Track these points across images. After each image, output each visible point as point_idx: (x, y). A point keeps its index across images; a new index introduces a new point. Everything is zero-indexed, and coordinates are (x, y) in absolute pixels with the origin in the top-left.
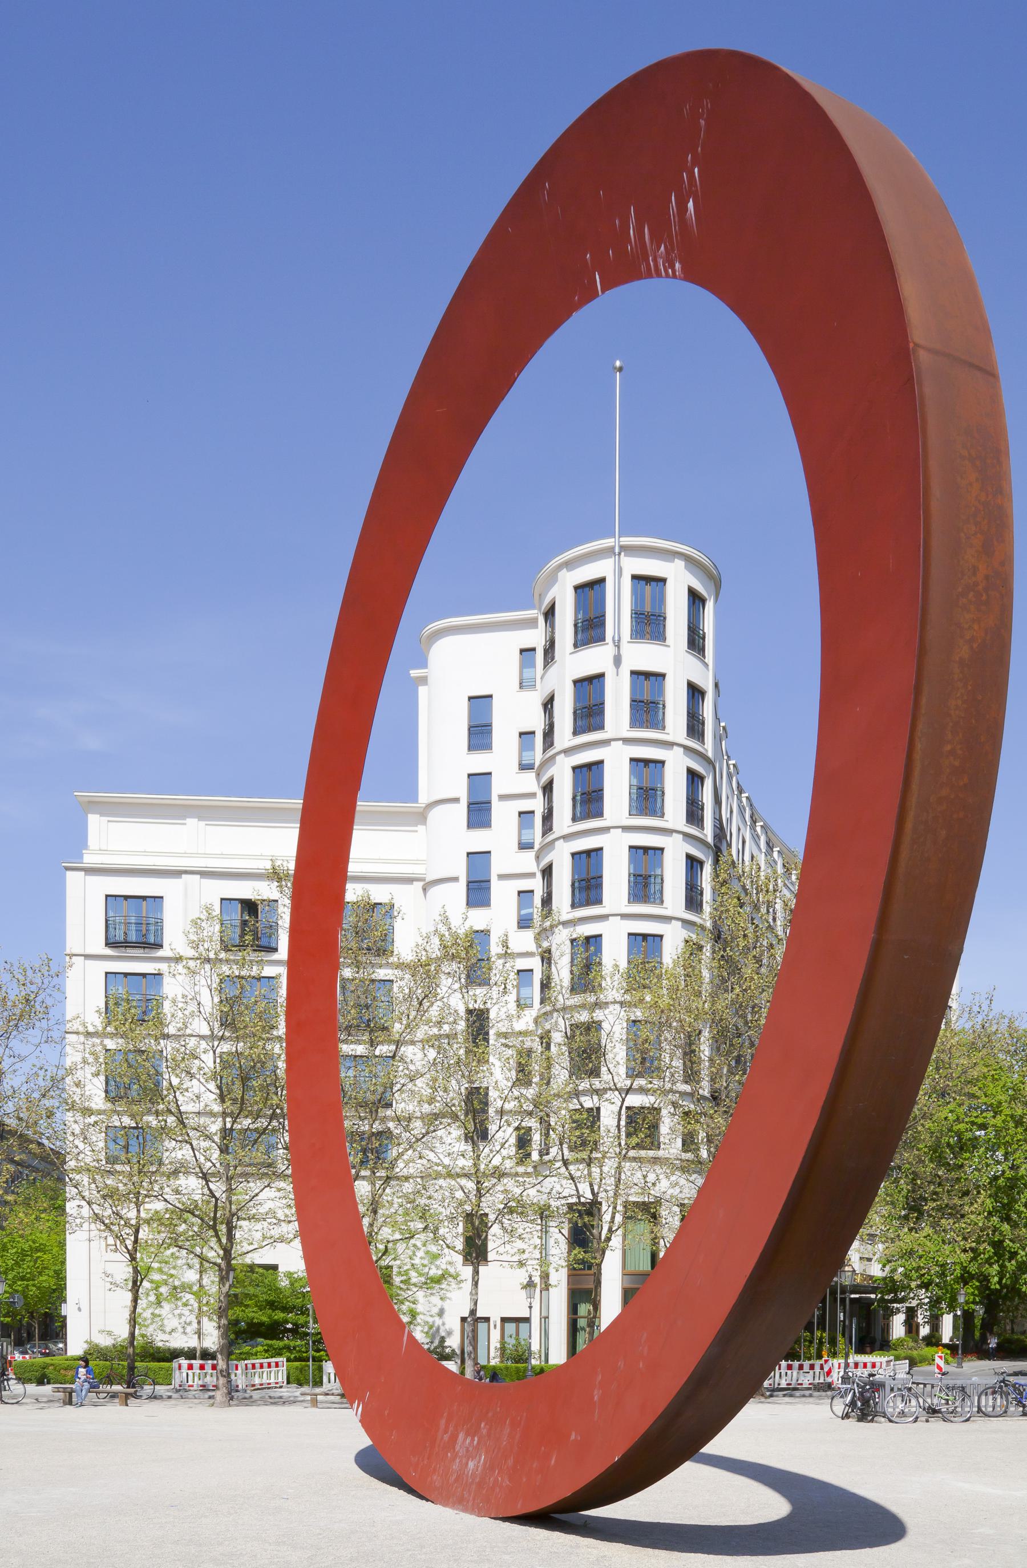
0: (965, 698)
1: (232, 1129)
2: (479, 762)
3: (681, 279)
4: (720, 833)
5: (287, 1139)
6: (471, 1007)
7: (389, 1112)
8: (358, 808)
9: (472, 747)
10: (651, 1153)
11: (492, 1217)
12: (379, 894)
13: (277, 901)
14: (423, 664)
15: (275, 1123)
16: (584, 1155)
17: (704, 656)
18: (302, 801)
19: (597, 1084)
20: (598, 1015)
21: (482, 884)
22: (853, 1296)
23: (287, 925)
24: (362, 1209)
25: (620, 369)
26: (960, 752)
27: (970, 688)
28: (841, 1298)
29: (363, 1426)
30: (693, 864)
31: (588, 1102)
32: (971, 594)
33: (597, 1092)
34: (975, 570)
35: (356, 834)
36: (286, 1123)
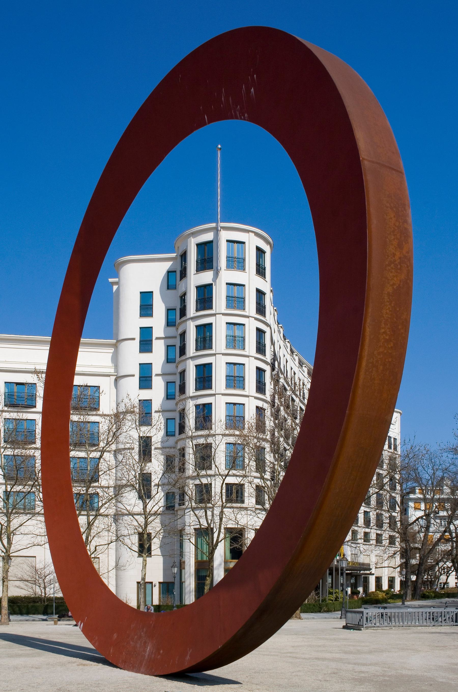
0: (391, 309)
1: (10, 492)
2: (146, 322)
3: (248, 121)
4: (275, 358)
5: (41, 497)
6: (141, 435)
7: (96, 484)
8: (81, 341)
9: (142, 315)
10: (239, 505)
11: (153, 535)
13: (36, 384)
14: (117, 275)
15: (34, 489)
16: (203, 505)
17: (265, 278)
18: (51, 338)
19: (209, 472)
21: (147, 378)
22: (347, 572)
23: (42, 395)
24: (82, 530)
25: (220, 149)
26: (389, 333)
27: (393, 305)
28: (341, 573)
30: (260, 371)
31: (204, 481)
32: (392, 265)
33: (210, 476)
34: (394, 255)
36: (41, 489)
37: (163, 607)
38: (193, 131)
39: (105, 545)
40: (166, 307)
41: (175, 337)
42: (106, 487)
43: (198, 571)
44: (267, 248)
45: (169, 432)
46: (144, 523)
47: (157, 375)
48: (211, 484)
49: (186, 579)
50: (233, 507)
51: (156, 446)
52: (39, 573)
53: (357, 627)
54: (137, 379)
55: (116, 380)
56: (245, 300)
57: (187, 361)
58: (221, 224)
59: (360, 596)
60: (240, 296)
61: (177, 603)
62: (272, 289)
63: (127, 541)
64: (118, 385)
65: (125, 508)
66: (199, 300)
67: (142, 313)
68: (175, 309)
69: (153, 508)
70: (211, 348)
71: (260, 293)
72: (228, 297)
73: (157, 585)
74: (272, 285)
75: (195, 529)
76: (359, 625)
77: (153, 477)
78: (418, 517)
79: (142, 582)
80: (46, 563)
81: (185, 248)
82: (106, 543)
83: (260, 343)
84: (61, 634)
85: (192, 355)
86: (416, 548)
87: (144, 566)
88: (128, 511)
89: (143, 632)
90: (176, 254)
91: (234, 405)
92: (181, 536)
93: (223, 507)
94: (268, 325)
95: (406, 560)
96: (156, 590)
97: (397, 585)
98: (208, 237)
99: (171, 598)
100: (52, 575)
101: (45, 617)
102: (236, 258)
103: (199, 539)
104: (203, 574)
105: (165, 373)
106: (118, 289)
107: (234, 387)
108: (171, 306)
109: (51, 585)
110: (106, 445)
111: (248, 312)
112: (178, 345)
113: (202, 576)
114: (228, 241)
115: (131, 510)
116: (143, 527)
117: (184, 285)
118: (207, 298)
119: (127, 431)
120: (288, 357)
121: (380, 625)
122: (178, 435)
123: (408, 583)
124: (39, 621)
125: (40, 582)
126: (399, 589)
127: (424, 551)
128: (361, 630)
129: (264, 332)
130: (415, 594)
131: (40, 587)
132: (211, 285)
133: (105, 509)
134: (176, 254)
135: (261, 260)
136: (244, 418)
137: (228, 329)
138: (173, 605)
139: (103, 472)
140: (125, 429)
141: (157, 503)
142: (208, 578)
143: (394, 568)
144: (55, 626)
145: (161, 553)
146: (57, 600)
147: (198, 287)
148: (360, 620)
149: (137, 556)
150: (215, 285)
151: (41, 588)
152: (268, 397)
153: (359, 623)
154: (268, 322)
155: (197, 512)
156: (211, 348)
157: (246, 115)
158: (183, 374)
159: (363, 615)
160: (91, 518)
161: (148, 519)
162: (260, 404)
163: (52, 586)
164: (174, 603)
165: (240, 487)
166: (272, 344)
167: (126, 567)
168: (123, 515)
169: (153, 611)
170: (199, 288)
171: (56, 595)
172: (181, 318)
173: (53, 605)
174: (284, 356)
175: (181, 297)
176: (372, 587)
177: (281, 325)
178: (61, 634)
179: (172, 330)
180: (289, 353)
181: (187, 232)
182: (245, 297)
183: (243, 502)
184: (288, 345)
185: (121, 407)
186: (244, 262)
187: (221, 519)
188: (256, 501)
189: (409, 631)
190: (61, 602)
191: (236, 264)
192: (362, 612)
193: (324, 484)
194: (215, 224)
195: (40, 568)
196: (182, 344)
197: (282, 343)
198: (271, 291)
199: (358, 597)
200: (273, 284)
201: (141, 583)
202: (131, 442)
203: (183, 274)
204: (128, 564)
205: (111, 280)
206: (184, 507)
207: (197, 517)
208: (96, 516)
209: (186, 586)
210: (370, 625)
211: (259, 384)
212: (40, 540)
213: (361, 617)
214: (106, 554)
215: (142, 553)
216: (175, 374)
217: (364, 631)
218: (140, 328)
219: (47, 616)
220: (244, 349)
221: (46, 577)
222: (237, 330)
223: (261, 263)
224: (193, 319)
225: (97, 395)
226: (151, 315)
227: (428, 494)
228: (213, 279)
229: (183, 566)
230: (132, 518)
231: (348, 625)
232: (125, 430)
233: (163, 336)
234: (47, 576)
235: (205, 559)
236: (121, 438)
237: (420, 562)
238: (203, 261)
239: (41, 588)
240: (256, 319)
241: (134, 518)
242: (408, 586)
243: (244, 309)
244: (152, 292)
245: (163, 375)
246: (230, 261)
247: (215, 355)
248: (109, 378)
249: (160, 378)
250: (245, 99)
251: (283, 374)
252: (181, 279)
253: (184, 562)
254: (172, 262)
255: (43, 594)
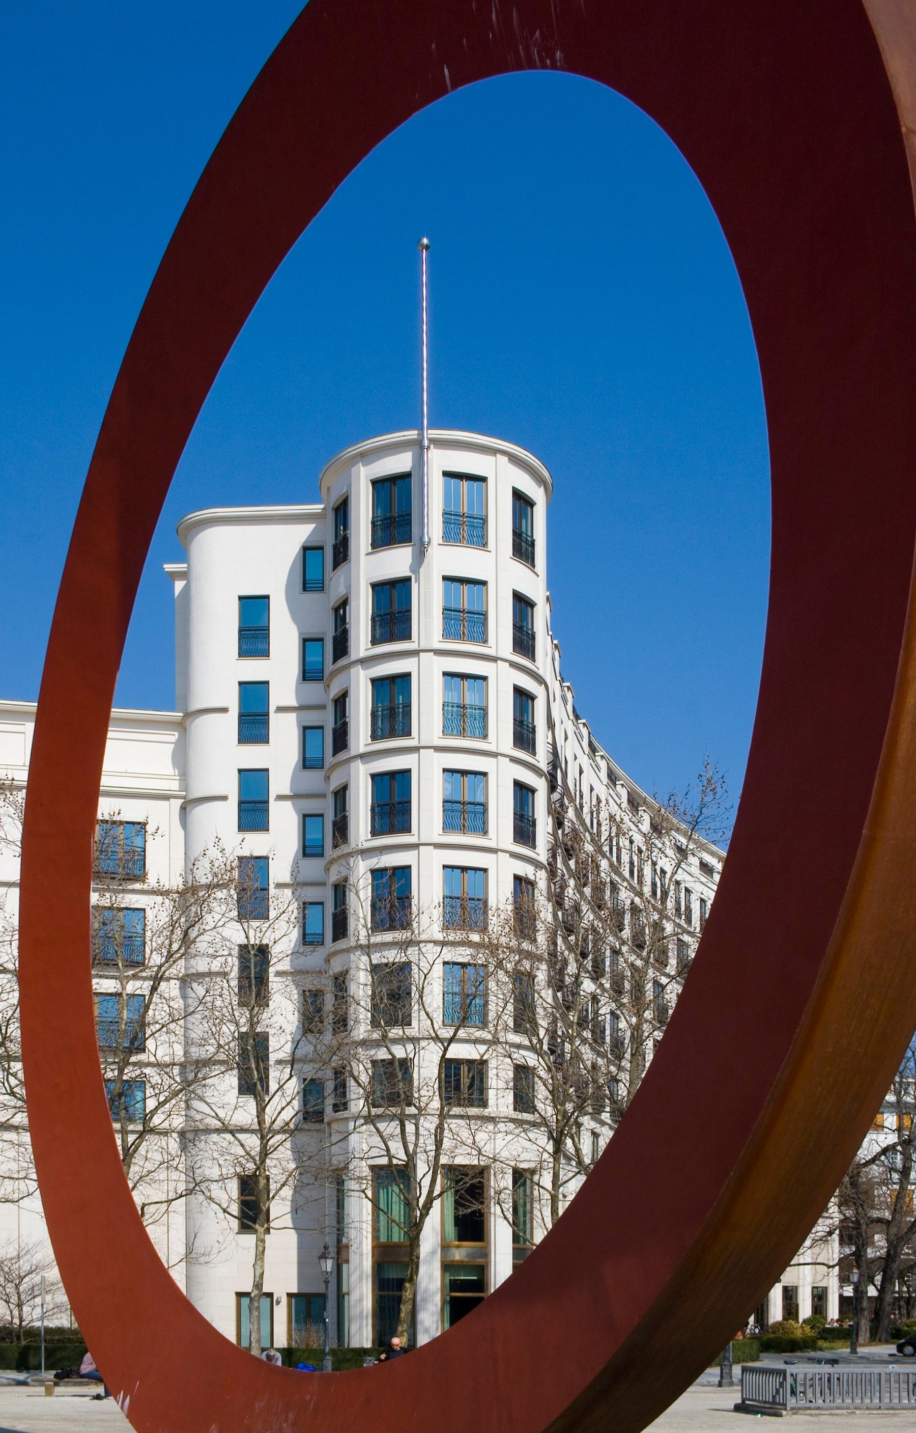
2: (254, 669)
3: (563, 69)
4: (555, 761)
7: (142, 1057)
8: (112, 715)
10: (473, 1111)
12: (131, 811)
14: (183, 555)
17: (534, 566)
18: (36, 704)
20: (412, 952)
21: (257, 805)
25: (427, 247)
29: (132, 1422)
30: (523, 791)
31: (399, 1052)
35: (110, 746)
37: (298, 1354)
38: (410, 114)
39: (161, 1202)
40: (300, 634)
41: (323, 707)
42: (168, 1066)
43: (379, 1267)
44: (537, 494)
45: (310, 934)
46: (258, 1149)
47: (280, 798)
48: (412, 1060)
49: (352, 1287)
50: (469, 1117)
51: (281, 967)
52: (6, 1269)
53: (771, 1408)
54: (232, 806)
55: (183, 808)
56: (486, 619)
57: (352, 764)
58: (430, 432)
59: (748, 1331)
60: (476, 609)
61: (332, 1344)
62: (548, 593)
63: (216, 1191)
64: (189, 820)
65: (213, 1114)
66: (379, 616)
67: (245, 647)
68: (321, 640)
69: (280, 1113)
70: (407, 733)
71: (522, 604)
72: (446, 610)
73: (284, 1300)
74: (550, 585)
75: (372, 1168)
76: (774, 1402)
77: (273, 1043)
78: (884, 1145)
79: (256, 1292)
80: (23, 1246)
81: (345, 490)
82: (164, 1198)
83: (521, 722)
84: (65, 1420)
85: (362, 749)
86: (880, 1220)
87: (260, 1255)
88: (220, 1120)
89: (286, 1421)
90: (322, 506)
91: (463, 872)
92: (340, 1183)
93: (442, 1116)
94: (540, 680)
95: (858, 1249)
96: (281, 1313)
97: (833, 1305)
98: (400, 463)
99: (317, 1332)
100: (37, 1274)
101: (22, 1376)
102: (466, 517)
103: (381, 1191)
104: (393, 1274)
105: (300, 792)
106: (186, 590)
107: (463, 829)
108: (313, 631)
109: (34, 1297)
110: (167, 962)
111: (494, 648)
112: (330, 726)
113: (388, 1279)
114: (446, 474)
115: (228, 1118)
116: (257, 1158)
117: (342, 579)
118: (398, 613)
119: (215, 928)
120: (585, 761)
121: (809, 1405)
122: (331, 941)
123: (861, 1303)
124: (9, 1385)
125: (8, 1290)
126: (836, 1317)
127: (899, 1228)
128: (780, 1415)
129: (532, 698)
130: (877, 1328)
131: (7, 1302)
132: (407, 580)
133: (163, 1117)
134: (322, 506)
135: (524, 522)
136: (486, 902)
137: (447, 687)
138: (324, 1350)
139: (158, 1026)
140: (209, 920)
141: (290, 1102)
142: (407, 1285)
143: (829, 1267)
144: (48, 1399)
145: (293, 1223)
146: (50, 1334)
147: (375, 586)
148: (778, 1392)
149: (236, 1230)
150: (418, 580)
151: (12, 1306)
152: (542, 853)
153: (774, 1397)
154: (541, 672)
155: (382, 1126)
156: (407, 733)
157: (558, 54)
158: (341, 795)
159: (785, 1379)
160: (131, 1138)
161: (268, 1141)
162: (526, 870)
163: (38, 1300)
164: (325, 1346)
165: (479, 1068)
166: (549, 727)
167: (212, 1257)
168: (208, 1131)
169: (279, 1363)
170: (377, 587)
171: (46, 1323)
172: (335, 659)
173: (41, 1347)
174: (576, 758)
175: (336, 610)
176: (776, 1313)
177: (568, 684)
178: (65, 1420)
179: (315, 691)
180: (587, 753)
181: (350, 450)
182: (487, 612)
183: (484, 1104)
184: (585, 732)
185: (201, 868)
186: (485, 527)
187: (439, 1143)
188: (515, 1102)
189: (896, 1419)
190: (58, 1340)
191: (465, 531)
192: (784, 1373)
193: (798, 1030)
194: (416, 432)
195: (8, 1257)
196: (339, 723)
197: (570, 727)
198: (548, 599)
199: (744, 1333)
200: (552, 583)
201: (253, 1295)
202: (226, 953)
203: (340, 553)
204: (215, 1251)
205: (168, 567)
206: (345, 1114)
207: (381, 1137)
208: (141, 1135)
209: (352, 1302)
210: (803, 1403)
211: (521, 821)
212: (10, 1189)
213: (781, 1384)
214: (163, 1225)
215: (255, 1223)
216: (323, 796)
217: (787, 1417)
218: (240, 683)
219: (28, 1372)
220: (485, 737)
221: (22, 1278)
222: (469, 690)
223: (524, 529)
224: (365, 662)
225: (138, 842)
226: (265, 653)
227: (906, 1093)
228: (410, 567)
229: (344, 1256)
230: (232, 1139)
231: (747, 1402)
232: (212, 925)
233: (293, 703)
234: (25, 1277)
235: (395, 1239)
236: (202, 945)
237: (888, 1252)
238: (389, 521)
239: (12, 1306)
240: (513, 665)
241: (236, 1138)
242: (862, 1310)
243: (485, 641)
244: (267, 597)
245: (295, 797)
246: (451, 523)
247: (416, 749)
248: (166, 803)
249: (288, 804)
250: (555, 7)
251: (572, 800)
252: (336, 566)
253: (347, 1247)
254: (314, 525)
255: (16, 1321)
